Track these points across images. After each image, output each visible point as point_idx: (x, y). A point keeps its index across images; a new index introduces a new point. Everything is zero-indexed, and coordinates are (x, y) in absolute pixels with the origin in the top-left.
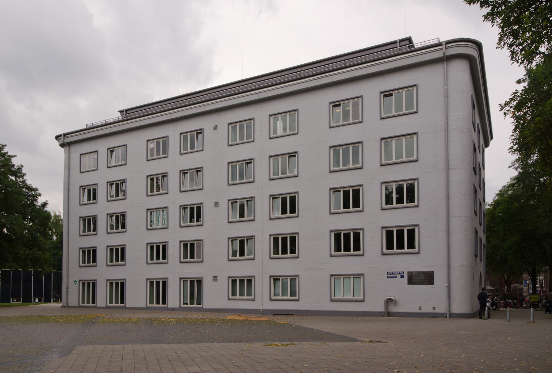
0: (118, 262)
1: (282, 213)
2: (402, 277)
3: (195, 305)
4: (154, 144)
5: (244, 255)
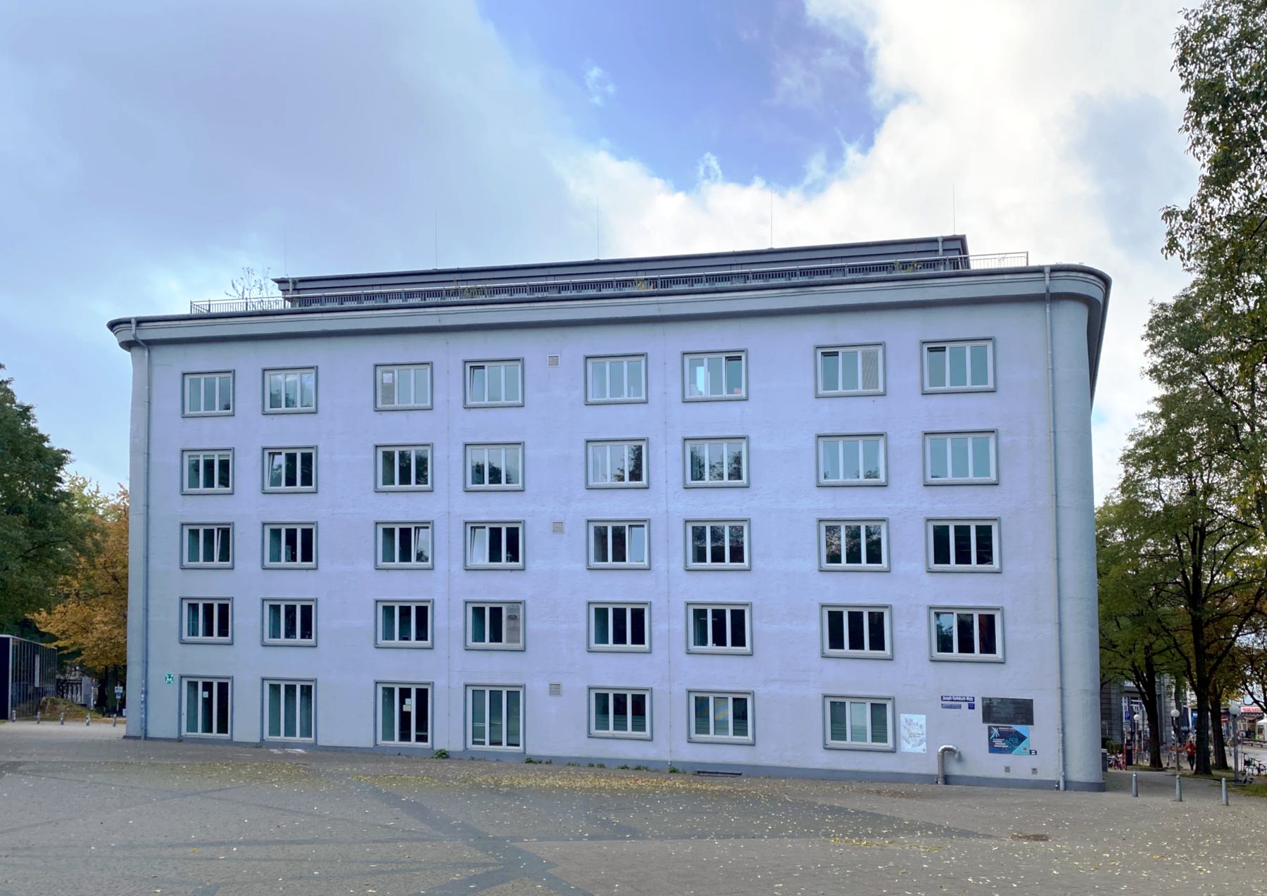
1: (491, 560)
2: (972, 707)
3: (215, 734)
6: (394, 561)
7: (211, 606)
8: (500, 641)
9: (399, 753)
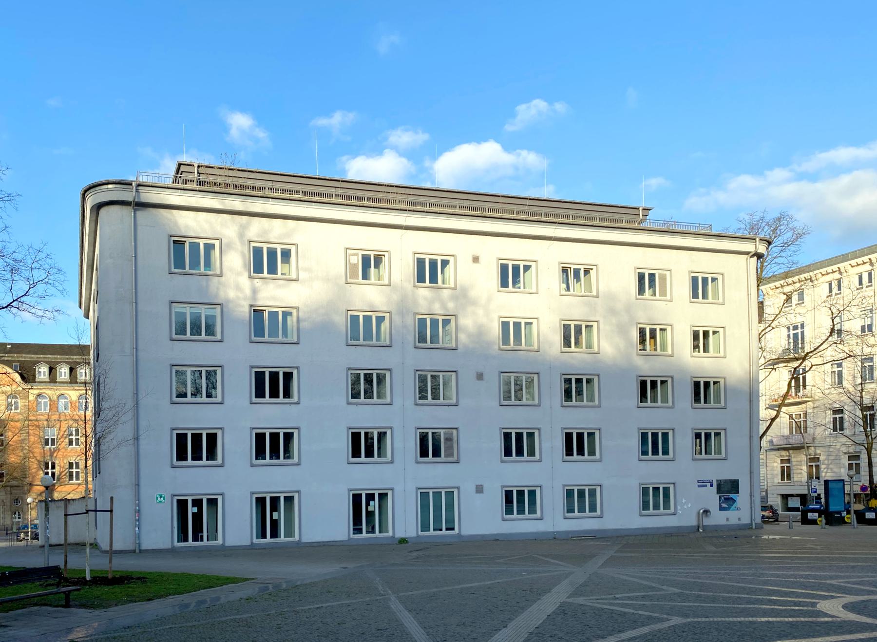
4: (358, 257)
6: (583, 402)
7: (657, 434)
8: (440, 456)
9: (263, 548)
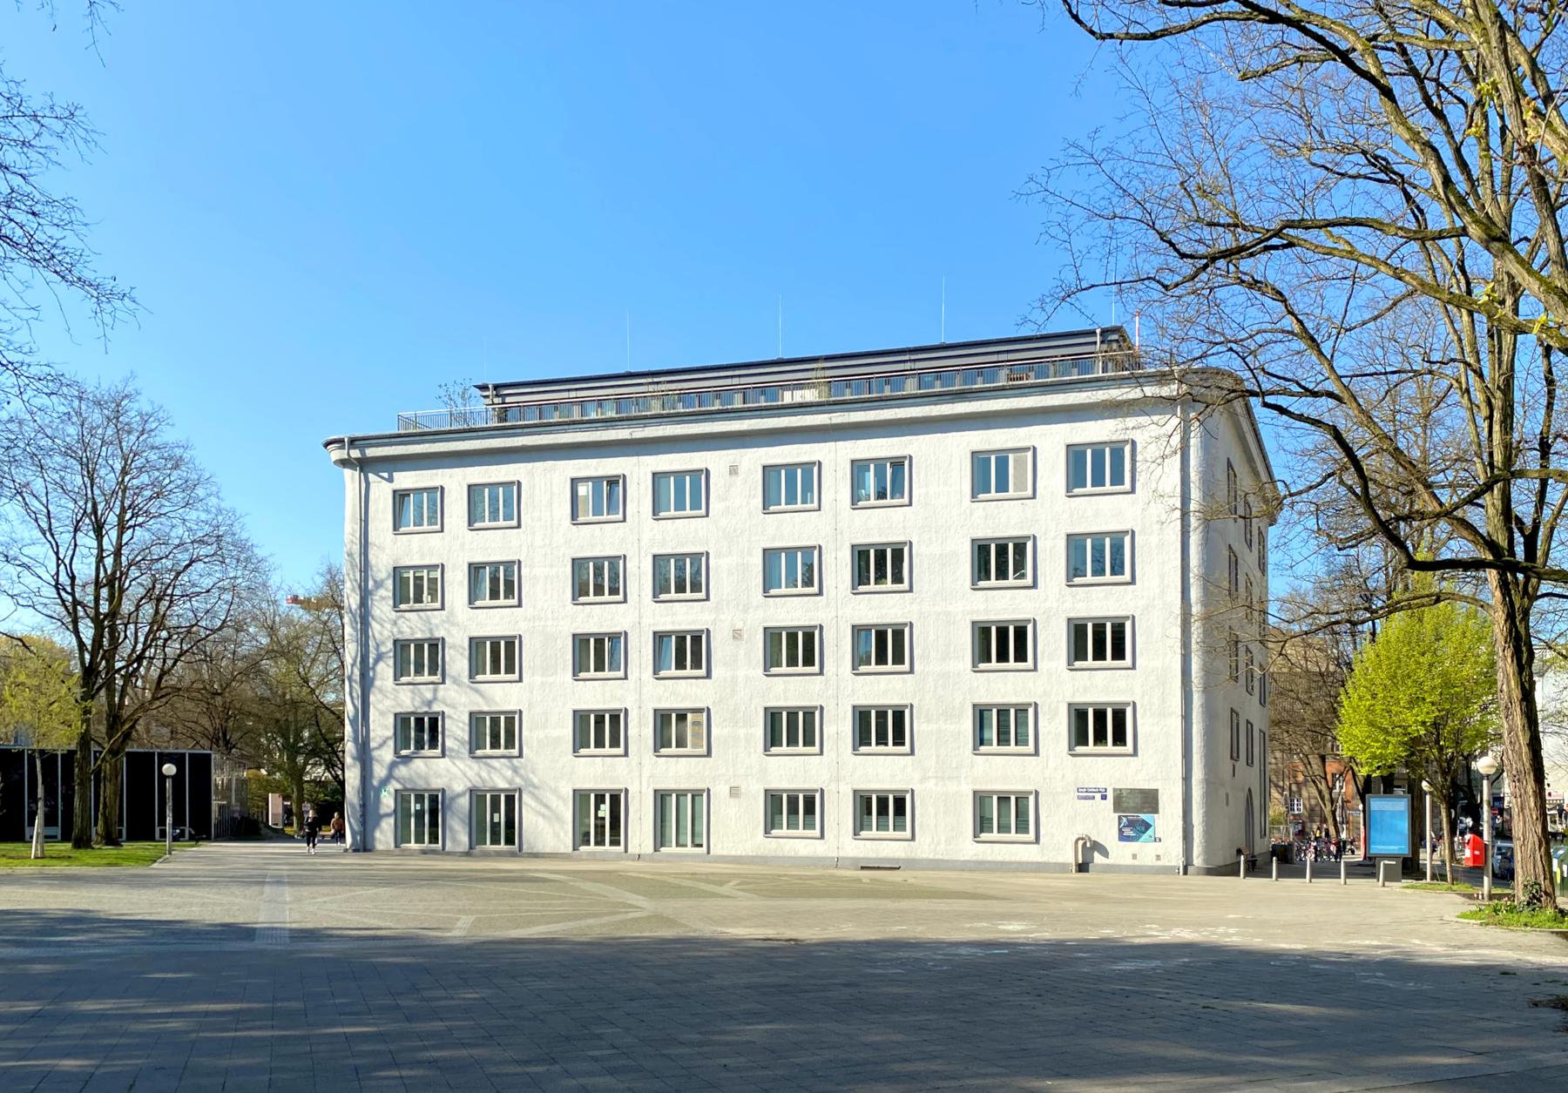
0: (684, 668)
2: (1104, 797)
5: (685, 746)
